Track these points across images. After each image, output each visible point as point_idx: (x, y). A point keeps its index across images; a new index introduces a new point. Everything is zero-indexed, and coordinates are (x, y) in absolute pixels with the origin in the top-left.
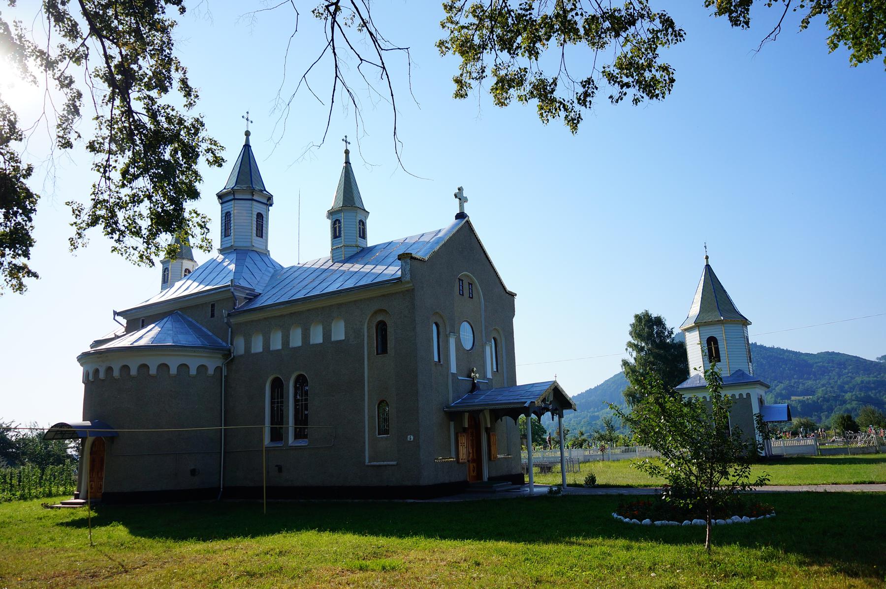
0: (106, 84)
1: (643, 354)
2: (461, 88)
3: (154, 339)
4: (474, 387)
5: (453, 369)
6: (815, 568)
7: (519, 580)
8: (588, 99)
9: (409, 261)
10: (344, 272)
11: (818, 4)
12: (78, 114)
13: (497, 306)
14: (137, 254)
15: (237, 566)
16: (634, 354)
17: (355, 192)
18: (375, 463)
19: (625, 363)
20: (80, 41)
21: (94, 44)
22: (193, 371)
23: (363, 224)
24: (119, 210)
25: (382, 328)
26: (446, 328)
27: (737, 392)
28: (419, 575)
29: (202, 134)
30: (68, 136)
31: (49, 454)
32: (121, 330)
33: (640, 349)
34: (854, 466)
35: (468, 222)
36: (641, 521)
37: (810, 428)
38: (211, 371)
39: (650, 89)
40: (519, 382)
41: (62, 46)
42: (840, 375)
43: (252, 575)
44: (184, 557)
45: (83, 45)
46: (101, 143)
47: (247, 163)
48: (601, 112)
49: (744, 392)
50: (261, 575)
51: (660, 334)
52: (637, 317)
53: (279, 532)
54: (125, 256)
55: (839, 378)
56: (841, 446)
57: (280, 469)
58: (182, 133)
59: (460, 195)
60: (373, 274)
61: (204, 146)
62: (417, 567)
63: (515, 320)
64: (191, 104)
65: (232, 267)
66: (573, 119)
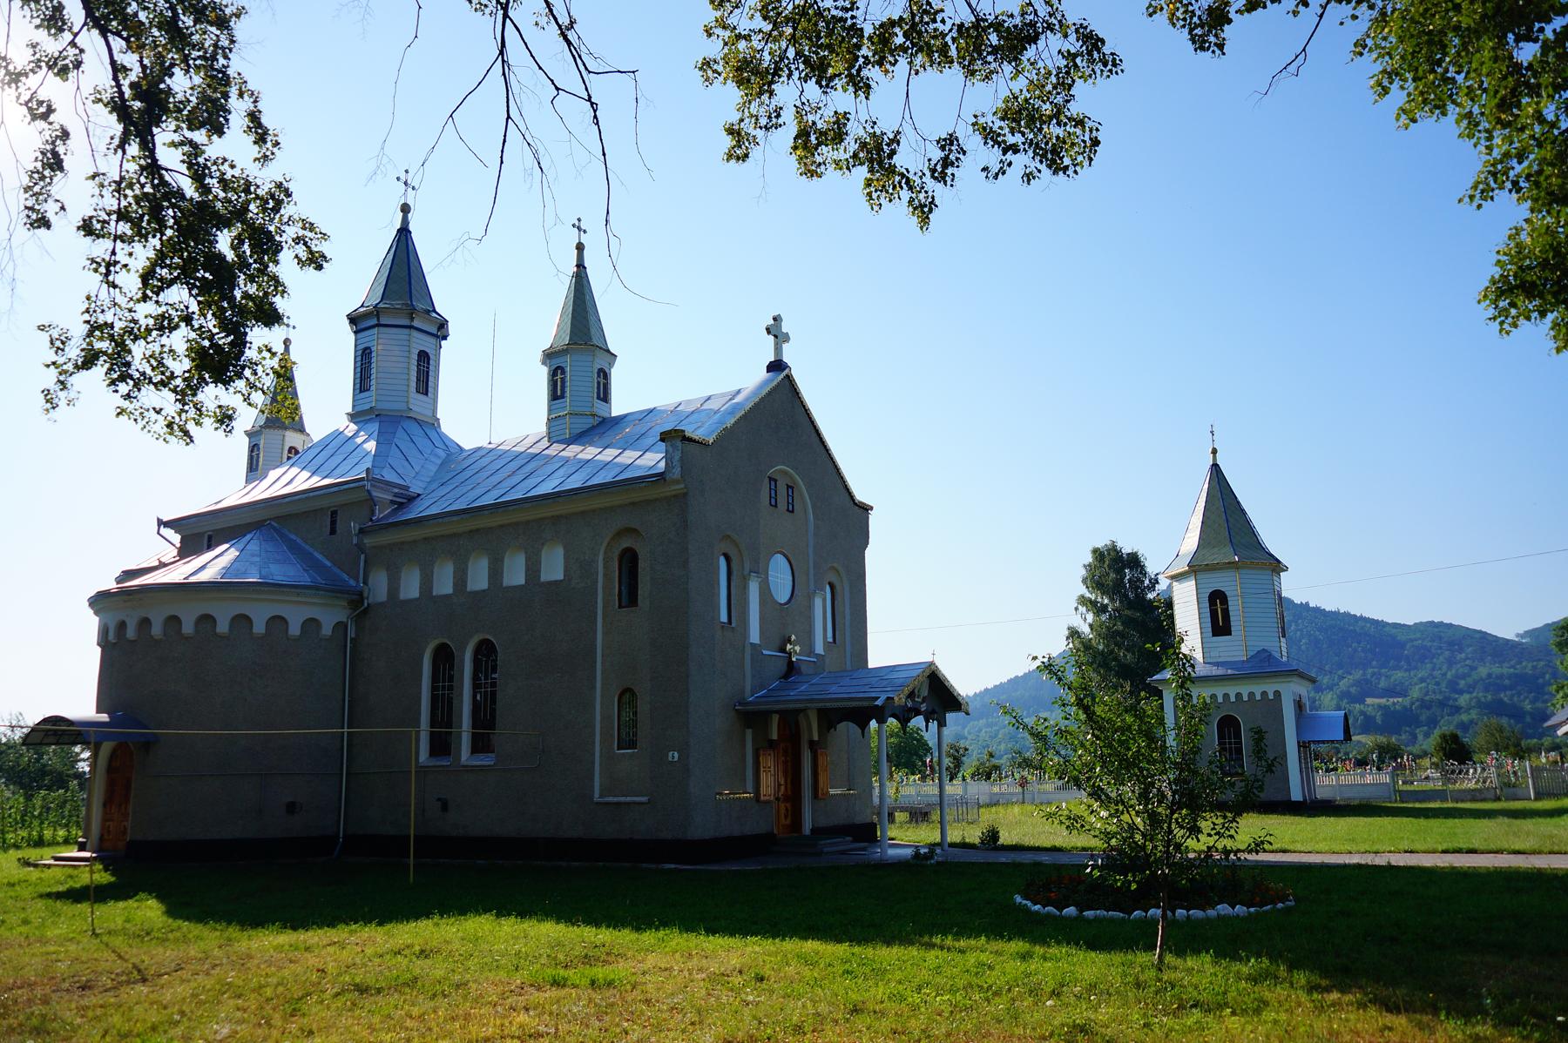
0: (114, 117)
1: (1104, 617)
2: (740, 144)
3: (227, 571)
4: (791, 669)
5: (755, 636)
6: (1335, 996)
7: (823, 1008)
8: (949, 171)
9: (679, 444)
10: (567, 460)
11: (1498, 9)
12: (61, 169)
13: (837, 527)
14: (162, 422)
15: (339, 975)
16: (1090, 617)
17: (592, 319)
18: (611, 799)
19: (1074, 634)
20: (67, 36)
21: (91, 40)
22: (295, 630)
23: (604, 375)
24: (134, 341)
25: (629, 561)
26: (744, 563)
27: (1257, 689)
28: (653, 995)
29: (287, 211)
30: (44, 207)
31: (44, 771)
32: (171, 553)
33: (1099, 609)
34: (1450, 822)
35: (789, 378)
36: (1061, 910)
37: (1388, 754)
38: (327, 630)
39: (1053, 157)
40: (874, 661)
41: (34, 46)
42: (1451, 662)
43: (362, 990)
44: (250, 957)
45: (73, 44)
46: (104, 222)
47: (403, 266)
48: (967, 196)
49: (1270, 688)
50: (379, 991)
51: (1136, 584)
52: (1097, 553)
53: (427, 915)
54: (141, 423)
55: (1450, 668)
56: (1439, 785)
57: (445, 806)
58: (252, 207)
59: (775, 330)
60: (618, 465)
61: (292, 231)
62: (651, 983)
63: (870, 554)
64: (265, 156)
65: (371, 446)
66: (922, 206)
